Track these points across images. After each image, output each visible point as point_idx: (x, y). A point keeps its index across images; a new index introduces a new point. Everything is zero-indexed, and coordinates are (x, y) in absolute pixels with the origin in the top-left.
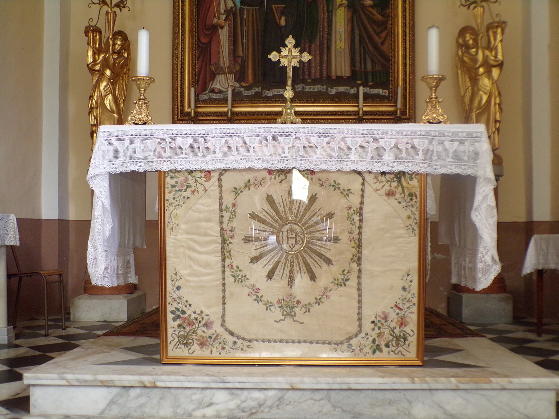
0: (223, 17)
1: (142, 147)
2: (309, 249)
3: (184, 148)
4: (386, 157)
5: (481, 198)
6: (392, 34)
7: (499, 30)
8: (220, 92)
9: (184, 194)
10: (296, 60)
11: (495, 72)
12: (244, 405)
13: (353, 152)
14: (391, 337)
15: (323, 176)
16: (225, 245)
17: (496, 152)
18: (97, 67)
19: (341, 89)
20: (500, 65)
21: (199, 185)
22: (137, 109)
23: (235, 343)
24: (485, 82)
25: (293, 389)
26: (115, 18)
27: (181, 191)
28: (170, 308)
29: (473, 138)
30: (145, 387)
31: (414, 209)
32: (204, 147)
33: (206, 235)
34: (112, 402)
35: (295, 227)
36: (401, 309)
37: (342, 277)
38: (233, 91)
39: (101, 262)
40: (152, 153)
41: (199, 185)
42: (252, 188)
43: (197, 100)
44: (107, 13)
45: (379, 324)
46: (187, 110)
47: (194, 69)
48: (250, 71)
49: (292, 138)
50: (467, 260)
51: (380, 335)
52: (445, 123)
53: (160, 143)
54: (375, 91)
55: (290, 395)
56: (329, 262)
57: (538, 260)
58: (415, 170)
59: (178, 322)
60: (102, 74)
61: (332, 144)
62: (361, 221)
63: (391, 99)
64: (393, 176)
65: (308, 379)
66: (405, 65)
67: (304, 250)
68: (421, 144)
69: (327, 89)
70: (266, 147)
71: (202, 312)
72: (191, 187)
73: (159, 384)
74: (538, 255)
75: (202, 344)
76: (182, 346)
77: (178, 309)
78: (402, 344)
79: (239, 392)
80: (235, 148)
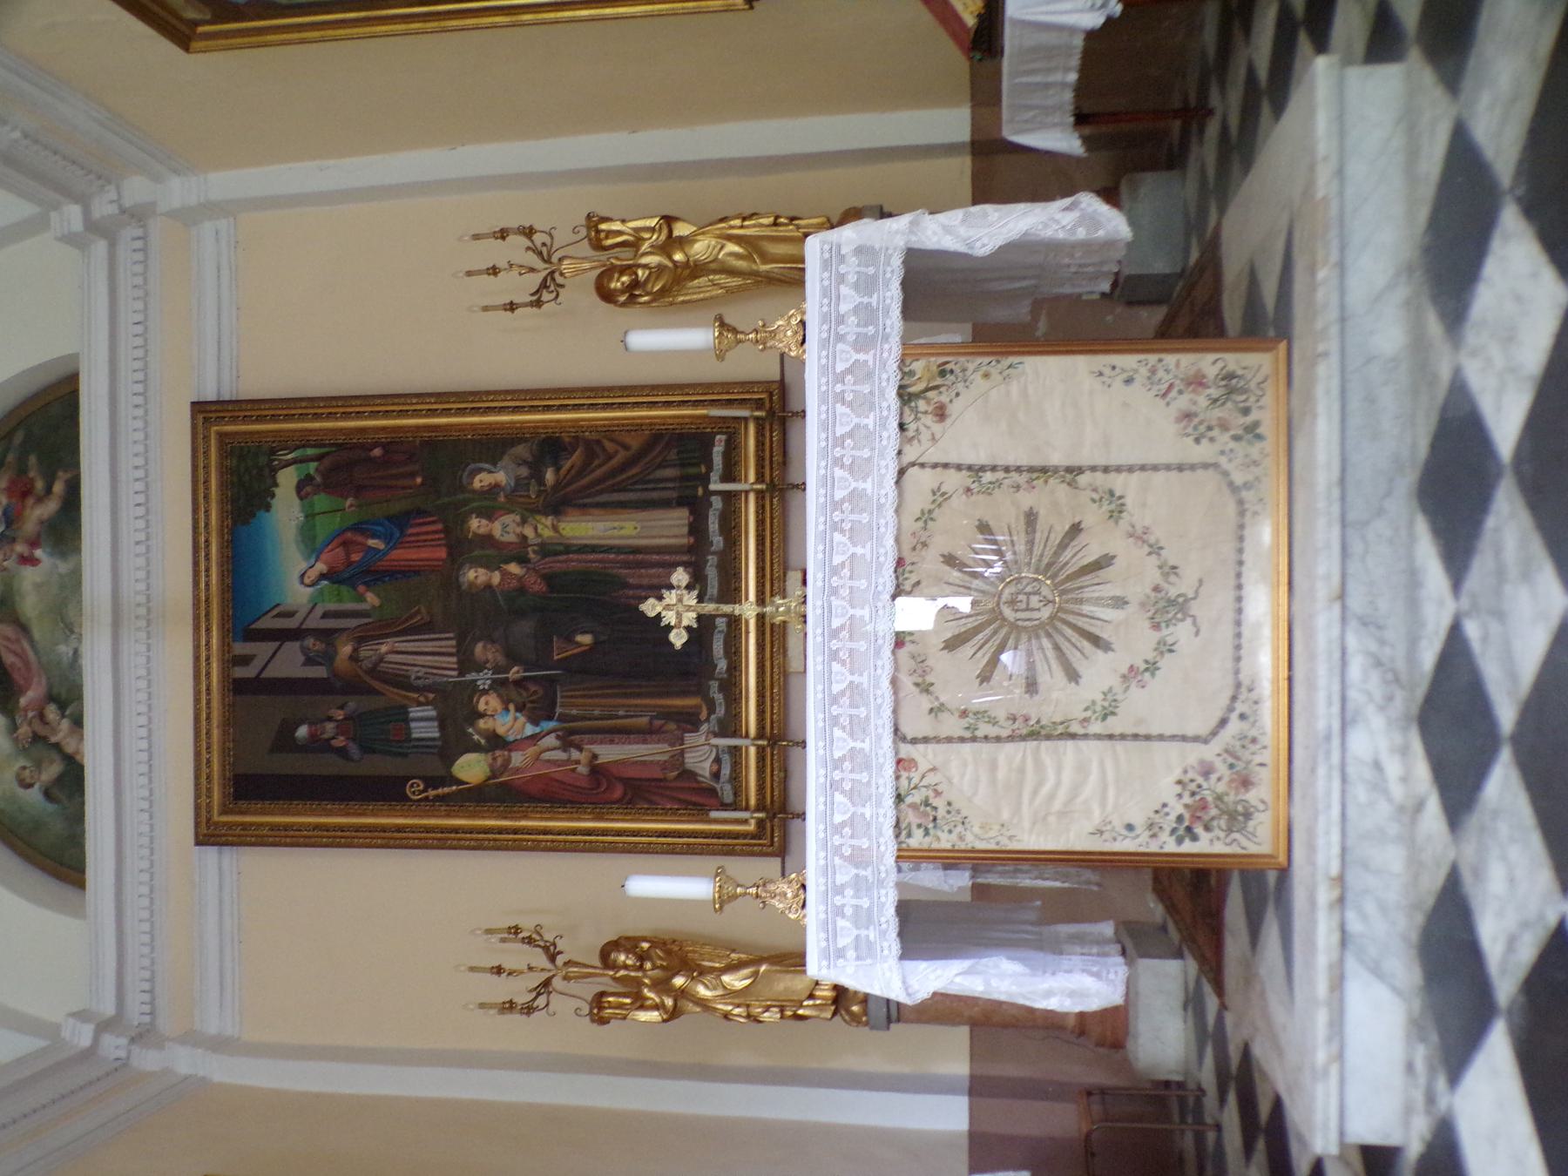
0: (575, 754)
1: (849, 892)
3: (853, 809)
4: (869, 421)
5: (949, 238)
6: (610, 431)
7: (603, 226)
8: (718, 760)
9: (941, 813)
10: (686, 597)
11: (681, 230)
13: (861, 485)
14: (1229, 404)
15: (907, 543)
16: (1043, 732)
17: (835, 220)
18: (669, 1002)
19: (713, 525)
20: (669, 220)
22: (775, 902)
23: (1242, 717)
24: (701, 248)
25: (1342, 596)
26: (576, 964)
27: (935, 819)
28: (1171, 847)
29: (834, 258)
30: (1341, 900)
31: (971, 367)
32: (852, 771)
33: (1022, 770)
34: (1376, 971)
35: (1004, 598)
36: (1171, 386)
37: (1105, 503)
38: (716, 735)
39: (1074, 984)
40: (863, 873)
42: (929, 679)
43: (734, 806)
44: (566, 978)
45: (1202, 428)
46: (751, 827)
47: (674, 812)
48: (678, 702)
49: (835, 602)
50: (1067, 261)
51: (1224, 426)
52: (804, 313)
53: (842, 856)
54: (718, 460)
55: (1356, 603)
56: (1076, 529)
57: (1055, 125)
58: (895, 366)
59: (1199, 830)
60: (681, 994)
61: (847, 526)
62: (994, 469)
63: (732, 429)
64: (906, 409)
65: (1323, 568)
66: (668, 404)
67: (1052, 577)
68: (846, 356)
69: (714, 553)
70: (851, 651)
71: (1179, 782)
72: (927, 799)
73: (1335, 870)
74: (1042, 126)
75: (1246, 783)
76: (1251, 824)
77: (1174, 831)
78: (1242, 383)
79: (1350, 706)
80: (854, 712)
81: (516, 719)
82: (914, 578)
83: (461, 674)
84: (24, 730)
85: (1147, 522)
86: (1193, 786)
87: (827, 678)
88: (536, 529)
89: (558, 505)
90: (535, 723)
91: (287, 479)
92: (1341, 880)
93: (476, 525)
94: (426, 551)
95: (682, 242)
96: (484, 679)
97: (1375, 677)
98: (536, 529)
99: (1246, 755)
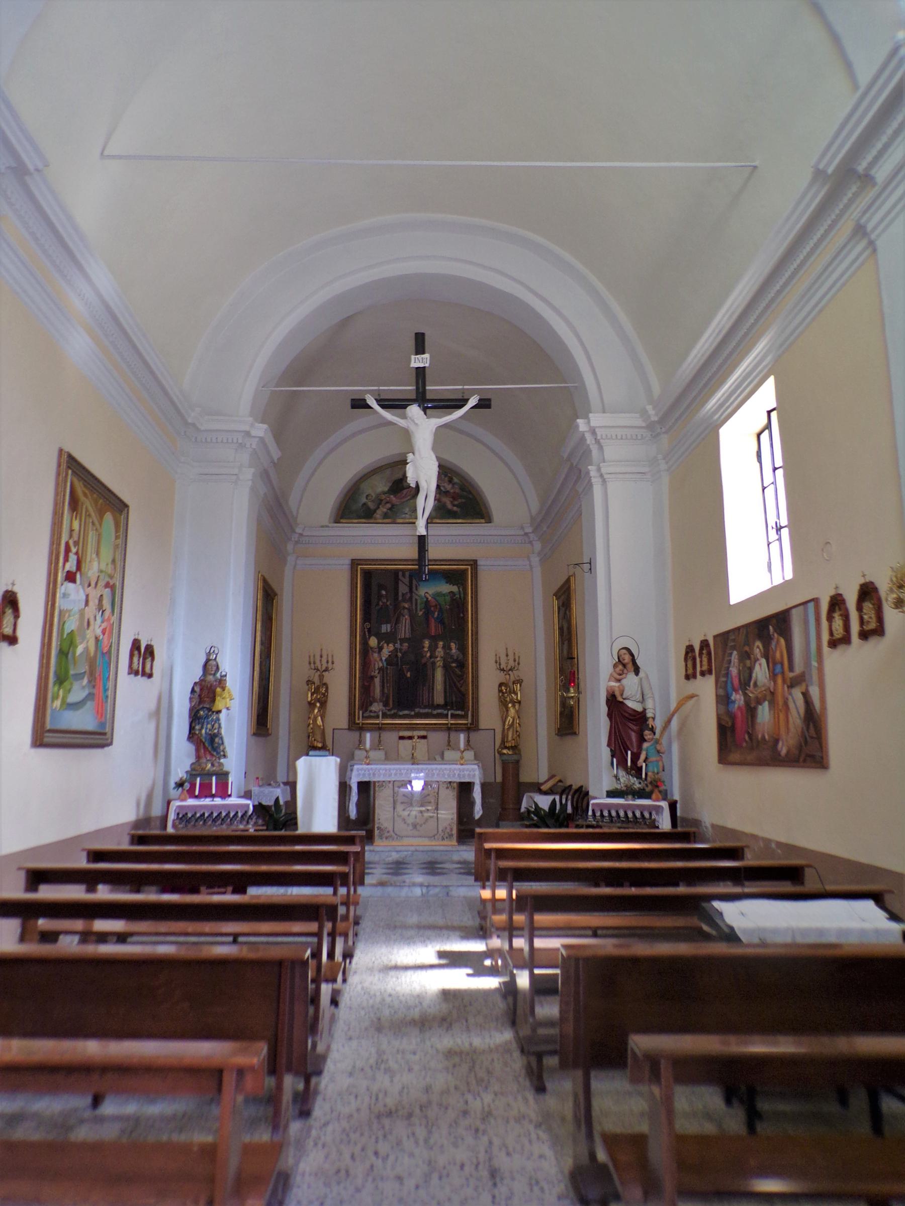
11: (517, 706)
19: (439, 711)
24: (512, 712)
29: (474, 770)
68: (457, 773)
83: (400, 639)
84: (383, 497)
89: (446, 667)
91: (455, 589)
93: (441, 644)
94: (434, 628)
95: (514, 706)
96: (398, 645)
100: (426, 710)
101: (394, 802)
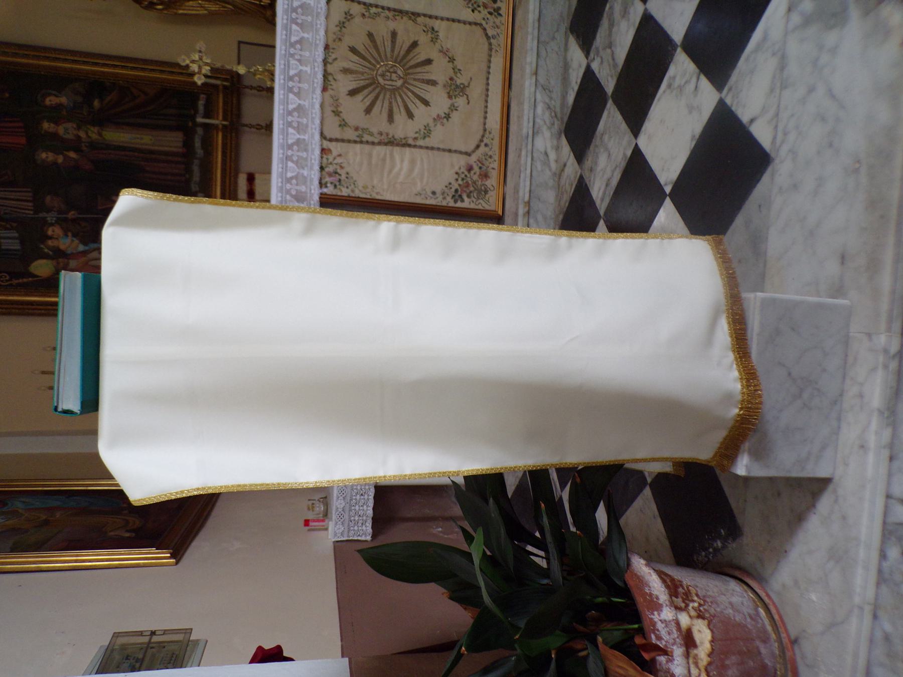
2: (401, 60)
9: (343, 177)
12: (548, 122)
15: (331, 37)
19: (198, 143)
21: (335, 162)
23: (486, 145)
25: (536, 74)
28: (452, 204)
30: (528, 212)
33: (384, 160)
41: (335, 162)
42: (340, 109)
45: (475, 6)
49: (292, 62)
55: (542, 79)
56: (415, 44)
59: (465, 197)
62: (377, 6)
73: (527, 199)
75: (485, 176)
77: (453, 196)
79: (537, 126)
81: (73, 241)
82: (334, 56)
85: (449, 46)
86: (463, 176)
87: (286, 102)
88: (87, 134)
89: (102, 120)
90: (85, 244)
92: (528, 203)
93: (46, 125)
96: (51, 217)
97: (547, 114)
98: (87, 134)
99: (487, 163)
100: (196, 169)
101: (391, 142)
